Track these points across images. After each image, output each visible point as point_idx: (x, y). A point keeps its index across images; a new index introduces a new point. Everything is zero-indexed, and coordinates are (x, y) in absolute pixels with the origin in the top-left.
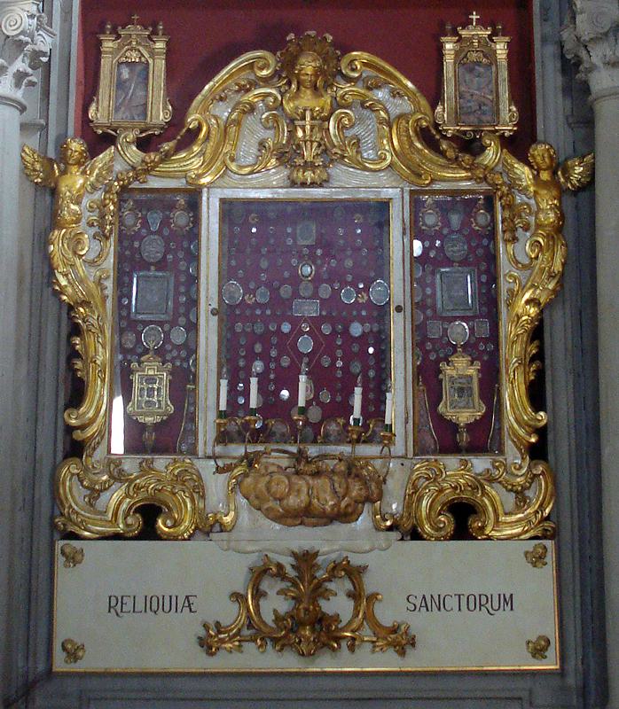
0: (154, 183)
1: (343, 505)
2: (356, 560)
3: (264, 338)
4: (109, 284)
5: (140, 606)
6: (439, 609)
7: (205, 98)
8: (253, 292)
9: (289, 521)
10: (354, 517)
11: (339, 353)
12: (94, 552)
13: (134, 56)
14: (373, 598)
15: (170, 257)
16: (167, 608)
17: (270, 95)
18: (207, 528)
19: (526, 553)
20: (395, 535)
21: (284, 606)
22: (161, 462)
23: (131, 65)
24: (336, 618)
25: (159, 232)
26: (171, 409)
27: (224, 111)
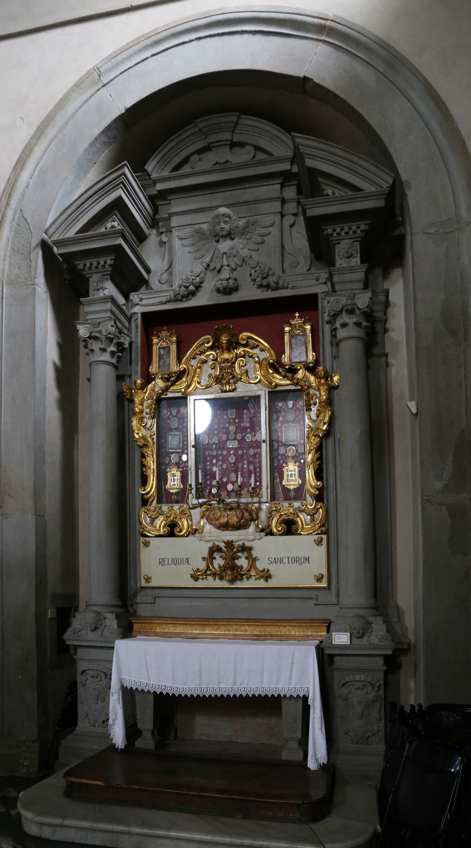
0: (170, 395)
1: (242, 521)
2: (248, 544)
3: (216, 457)
4: (155, 437)
5: (170, 562)
6: (281, 563)
7: (187, 358)
8: (212, 438)
9: (222, 529)
10: (247, 527)
11: (245, 462)
12: (154, 542)
13: (164, 344)
14: (255, 560)
15: (180, 426)
16: (180, 563)
17: (212, 354)
18: (193, 532)
19: (315, 540)
20: (263, 534)
21: (222, 562)
22: (176, 507)
23: (164, 348)
24: (241, 567)
25: (176, 416)
26: (182, 486)
27: (194, 363)
